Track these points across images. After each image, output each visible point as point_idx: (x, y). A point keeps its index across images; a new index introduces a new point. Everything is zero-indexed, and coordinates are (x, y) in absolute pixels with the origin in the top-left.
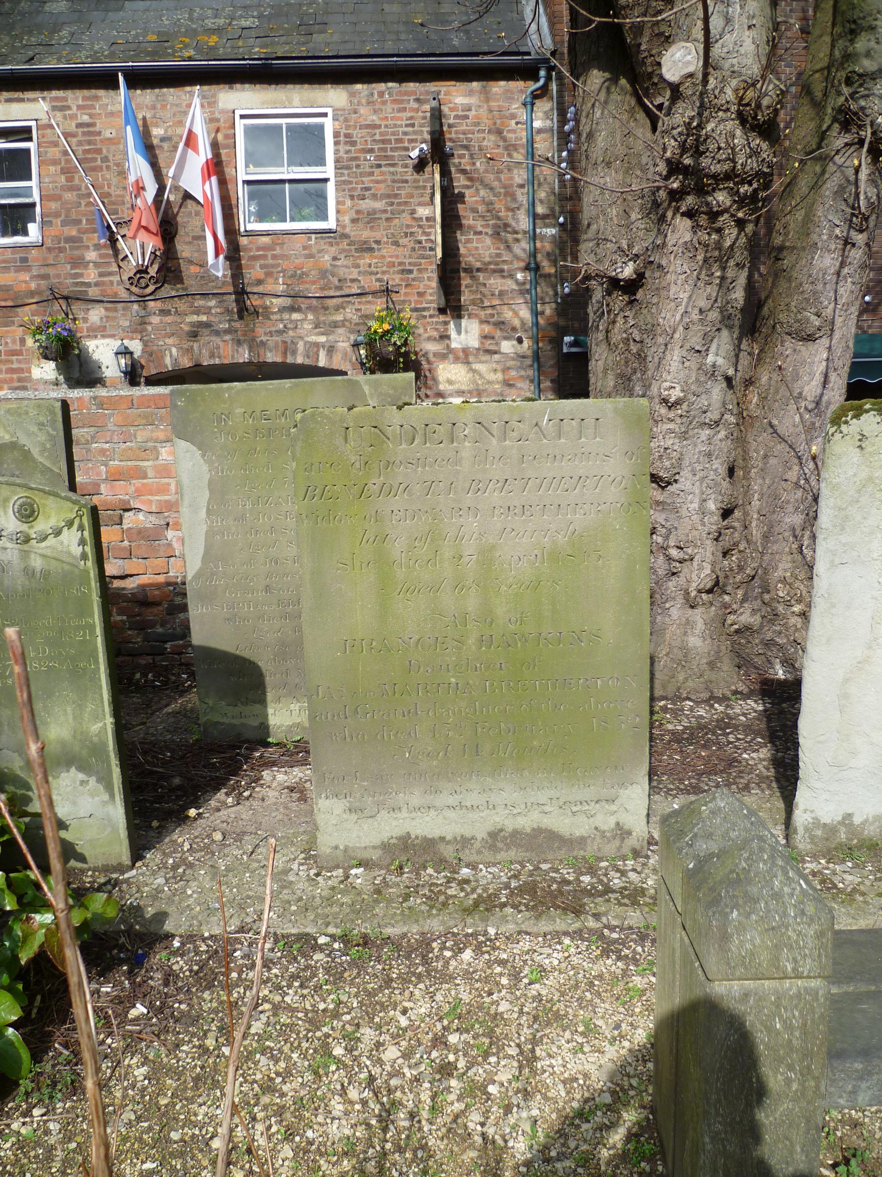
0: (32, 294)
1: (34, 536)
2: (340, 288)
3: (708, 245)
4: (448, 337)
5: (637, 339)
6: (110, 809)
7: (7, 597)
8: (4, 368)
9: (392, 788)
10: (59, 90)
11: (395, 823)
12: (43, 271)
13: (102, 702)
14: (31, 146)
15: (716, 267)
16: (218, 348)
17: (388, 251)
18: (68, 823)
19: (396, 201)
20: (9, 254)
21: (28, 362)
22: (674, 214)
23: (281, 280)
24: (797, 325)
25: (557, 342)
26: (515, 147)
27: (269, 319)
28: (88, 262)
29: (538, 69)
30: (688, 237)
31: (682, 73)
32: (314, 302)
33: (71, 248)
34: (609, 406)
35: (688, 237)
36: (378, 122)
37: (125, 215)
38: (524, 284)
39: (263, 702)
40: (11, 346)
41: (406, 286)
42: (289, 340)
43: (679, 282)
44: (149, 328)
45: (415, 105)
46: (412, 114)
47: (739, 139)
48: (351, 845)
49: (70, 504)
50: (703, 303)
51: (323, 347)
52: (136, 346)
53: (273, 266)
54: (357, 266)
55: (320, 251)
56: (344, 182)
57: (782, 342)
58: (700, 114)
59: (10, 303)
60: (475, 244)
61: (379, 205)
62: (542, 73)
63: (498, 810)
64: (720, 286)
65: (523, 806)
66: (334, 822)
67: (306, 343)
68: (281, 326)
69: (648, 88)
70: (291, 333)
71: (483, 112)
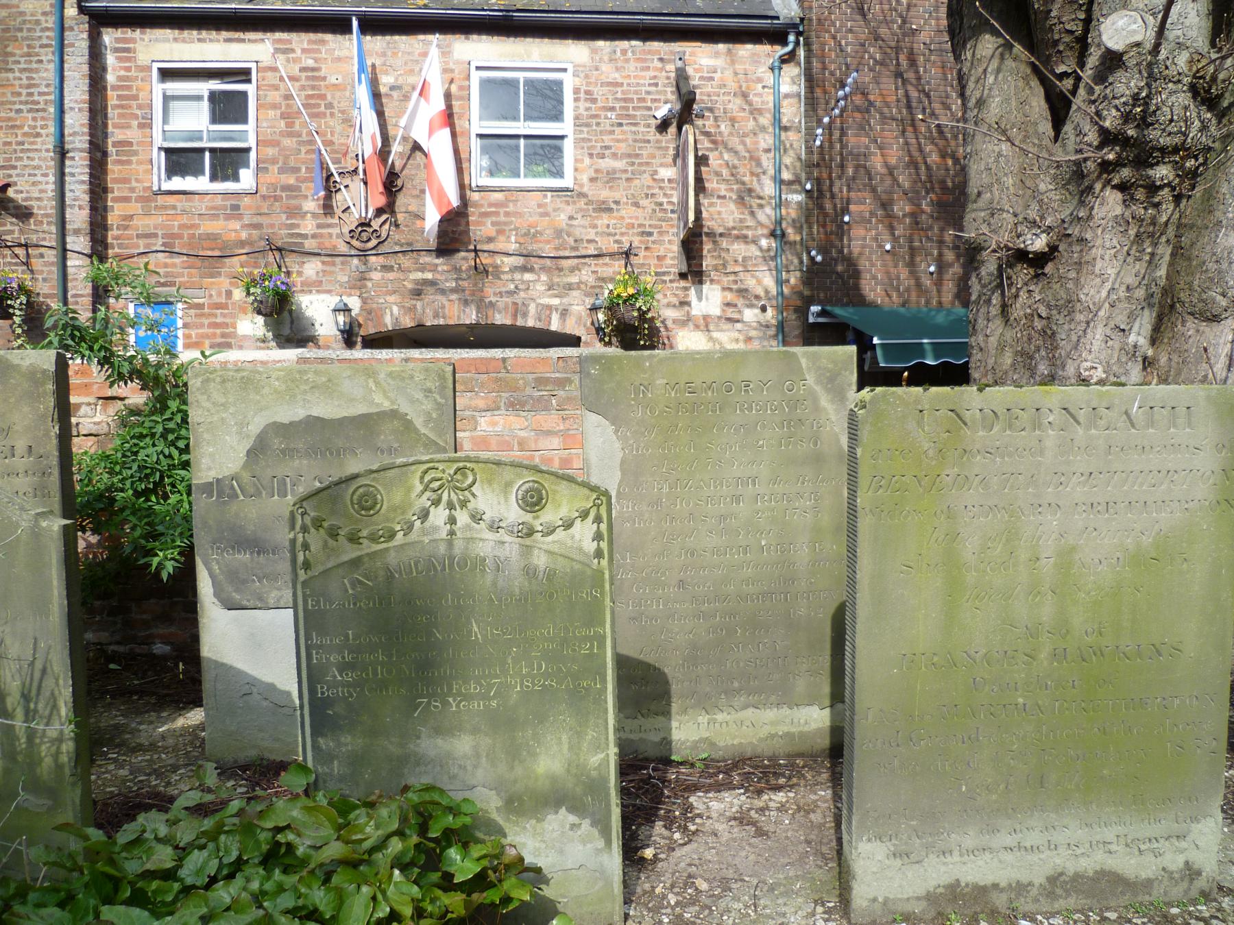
0: (242, 244)
1: (540, 528)
2: (576, 249)
3: (1143, 220)
4: (688, 304)
5: (1044, 315)
6: (605, 858)
7: (500, 601)
8: (206, 322)
9: (944, 828)
10: (283, 31)
11: (943, 869)
12: (256, 220)
13: (607, 729)
14: (250, 89)
15: (1147, 243)
16: (443, 307)
17: (627, 212)
18: (550, 876)
19: (637, 161)
20: (219, 201)
21: (233, 316)
22: (1104, 187)
23: (513, 239)
24: (1200, 305)
25: (802, 312)
26: (760, 111)
27: (500, 279)
28: (306, 213)
29: (787, 34)
30: (1119, 210)
31: (1128, 42)
32: (548, 262)
33: (288, 197)
34: (1202, 393)
35: (1119, 210)
36: (620, 80)
37: (349, 165)
38: (769, 250)
39: (667, 713)
40: (216, 299)
41: (646, 248)
42: (519, 302)
43: (1107, 257)
44: (369, 284)
45: (659, 65)
46: (643, 73)
47: (1193, 113)
48: (891, 897)
49: (586, 491)
50: (1131, 280)
51: (557, 310)
52: (354, 303)
53: (505, 224)
54: (595, 227)
55: (555, 210)
56: (583, 139)
57: (1184, 322)
58: (1148, 85)
59: (217, 253)
60: (718, 208)
61: (619, 164)
62: (791, 38)
63: (1060, 850)
64: (1150, 262)
65: (1087, 845)
66: (875, 869)
67: (538, 305)
68: (512, 287)
69: (1050, 55)
70: (522, 294)
71: (729, 74)
